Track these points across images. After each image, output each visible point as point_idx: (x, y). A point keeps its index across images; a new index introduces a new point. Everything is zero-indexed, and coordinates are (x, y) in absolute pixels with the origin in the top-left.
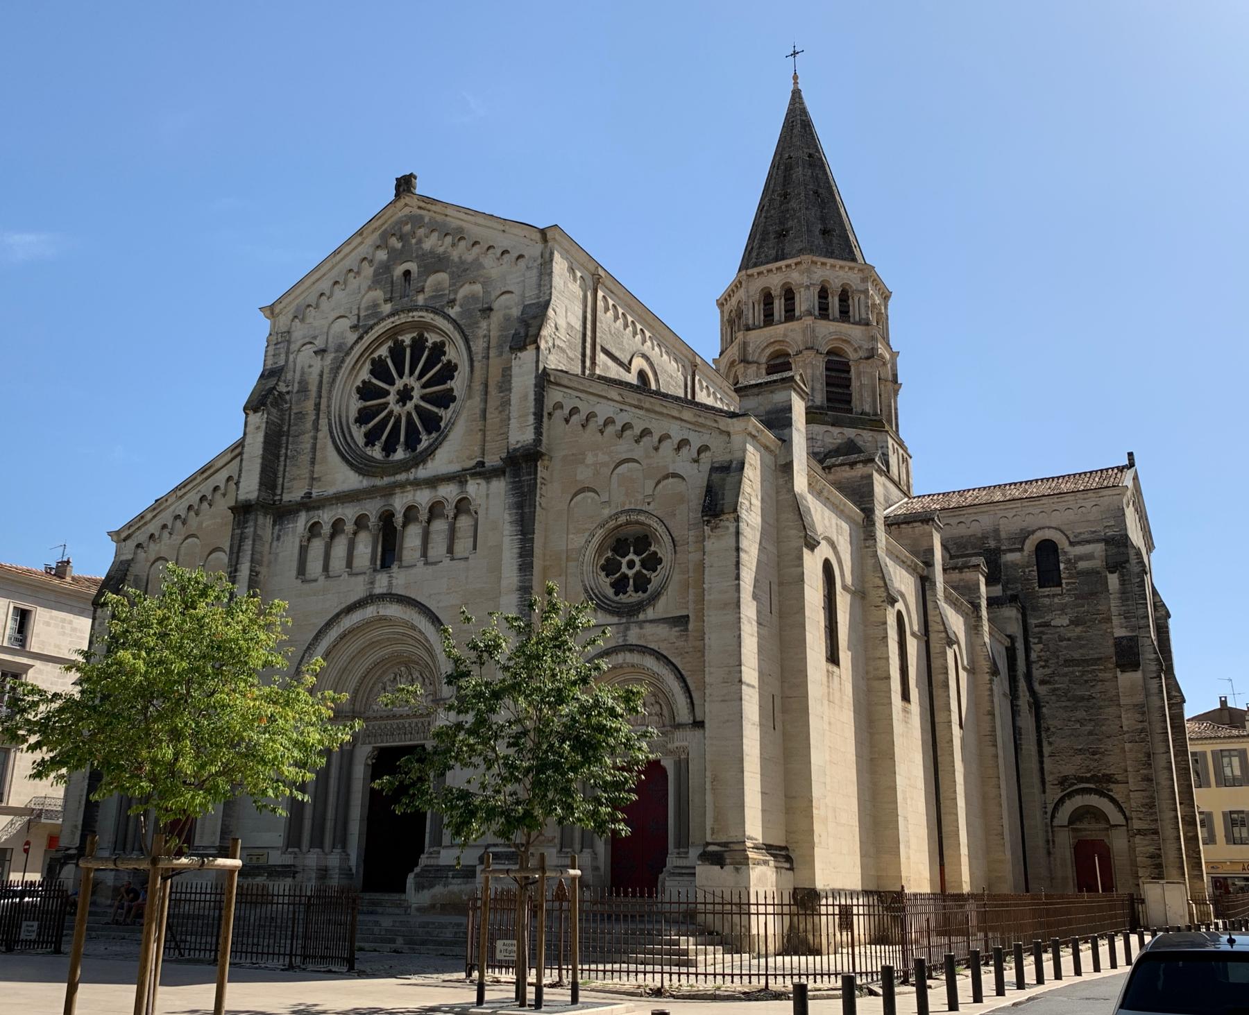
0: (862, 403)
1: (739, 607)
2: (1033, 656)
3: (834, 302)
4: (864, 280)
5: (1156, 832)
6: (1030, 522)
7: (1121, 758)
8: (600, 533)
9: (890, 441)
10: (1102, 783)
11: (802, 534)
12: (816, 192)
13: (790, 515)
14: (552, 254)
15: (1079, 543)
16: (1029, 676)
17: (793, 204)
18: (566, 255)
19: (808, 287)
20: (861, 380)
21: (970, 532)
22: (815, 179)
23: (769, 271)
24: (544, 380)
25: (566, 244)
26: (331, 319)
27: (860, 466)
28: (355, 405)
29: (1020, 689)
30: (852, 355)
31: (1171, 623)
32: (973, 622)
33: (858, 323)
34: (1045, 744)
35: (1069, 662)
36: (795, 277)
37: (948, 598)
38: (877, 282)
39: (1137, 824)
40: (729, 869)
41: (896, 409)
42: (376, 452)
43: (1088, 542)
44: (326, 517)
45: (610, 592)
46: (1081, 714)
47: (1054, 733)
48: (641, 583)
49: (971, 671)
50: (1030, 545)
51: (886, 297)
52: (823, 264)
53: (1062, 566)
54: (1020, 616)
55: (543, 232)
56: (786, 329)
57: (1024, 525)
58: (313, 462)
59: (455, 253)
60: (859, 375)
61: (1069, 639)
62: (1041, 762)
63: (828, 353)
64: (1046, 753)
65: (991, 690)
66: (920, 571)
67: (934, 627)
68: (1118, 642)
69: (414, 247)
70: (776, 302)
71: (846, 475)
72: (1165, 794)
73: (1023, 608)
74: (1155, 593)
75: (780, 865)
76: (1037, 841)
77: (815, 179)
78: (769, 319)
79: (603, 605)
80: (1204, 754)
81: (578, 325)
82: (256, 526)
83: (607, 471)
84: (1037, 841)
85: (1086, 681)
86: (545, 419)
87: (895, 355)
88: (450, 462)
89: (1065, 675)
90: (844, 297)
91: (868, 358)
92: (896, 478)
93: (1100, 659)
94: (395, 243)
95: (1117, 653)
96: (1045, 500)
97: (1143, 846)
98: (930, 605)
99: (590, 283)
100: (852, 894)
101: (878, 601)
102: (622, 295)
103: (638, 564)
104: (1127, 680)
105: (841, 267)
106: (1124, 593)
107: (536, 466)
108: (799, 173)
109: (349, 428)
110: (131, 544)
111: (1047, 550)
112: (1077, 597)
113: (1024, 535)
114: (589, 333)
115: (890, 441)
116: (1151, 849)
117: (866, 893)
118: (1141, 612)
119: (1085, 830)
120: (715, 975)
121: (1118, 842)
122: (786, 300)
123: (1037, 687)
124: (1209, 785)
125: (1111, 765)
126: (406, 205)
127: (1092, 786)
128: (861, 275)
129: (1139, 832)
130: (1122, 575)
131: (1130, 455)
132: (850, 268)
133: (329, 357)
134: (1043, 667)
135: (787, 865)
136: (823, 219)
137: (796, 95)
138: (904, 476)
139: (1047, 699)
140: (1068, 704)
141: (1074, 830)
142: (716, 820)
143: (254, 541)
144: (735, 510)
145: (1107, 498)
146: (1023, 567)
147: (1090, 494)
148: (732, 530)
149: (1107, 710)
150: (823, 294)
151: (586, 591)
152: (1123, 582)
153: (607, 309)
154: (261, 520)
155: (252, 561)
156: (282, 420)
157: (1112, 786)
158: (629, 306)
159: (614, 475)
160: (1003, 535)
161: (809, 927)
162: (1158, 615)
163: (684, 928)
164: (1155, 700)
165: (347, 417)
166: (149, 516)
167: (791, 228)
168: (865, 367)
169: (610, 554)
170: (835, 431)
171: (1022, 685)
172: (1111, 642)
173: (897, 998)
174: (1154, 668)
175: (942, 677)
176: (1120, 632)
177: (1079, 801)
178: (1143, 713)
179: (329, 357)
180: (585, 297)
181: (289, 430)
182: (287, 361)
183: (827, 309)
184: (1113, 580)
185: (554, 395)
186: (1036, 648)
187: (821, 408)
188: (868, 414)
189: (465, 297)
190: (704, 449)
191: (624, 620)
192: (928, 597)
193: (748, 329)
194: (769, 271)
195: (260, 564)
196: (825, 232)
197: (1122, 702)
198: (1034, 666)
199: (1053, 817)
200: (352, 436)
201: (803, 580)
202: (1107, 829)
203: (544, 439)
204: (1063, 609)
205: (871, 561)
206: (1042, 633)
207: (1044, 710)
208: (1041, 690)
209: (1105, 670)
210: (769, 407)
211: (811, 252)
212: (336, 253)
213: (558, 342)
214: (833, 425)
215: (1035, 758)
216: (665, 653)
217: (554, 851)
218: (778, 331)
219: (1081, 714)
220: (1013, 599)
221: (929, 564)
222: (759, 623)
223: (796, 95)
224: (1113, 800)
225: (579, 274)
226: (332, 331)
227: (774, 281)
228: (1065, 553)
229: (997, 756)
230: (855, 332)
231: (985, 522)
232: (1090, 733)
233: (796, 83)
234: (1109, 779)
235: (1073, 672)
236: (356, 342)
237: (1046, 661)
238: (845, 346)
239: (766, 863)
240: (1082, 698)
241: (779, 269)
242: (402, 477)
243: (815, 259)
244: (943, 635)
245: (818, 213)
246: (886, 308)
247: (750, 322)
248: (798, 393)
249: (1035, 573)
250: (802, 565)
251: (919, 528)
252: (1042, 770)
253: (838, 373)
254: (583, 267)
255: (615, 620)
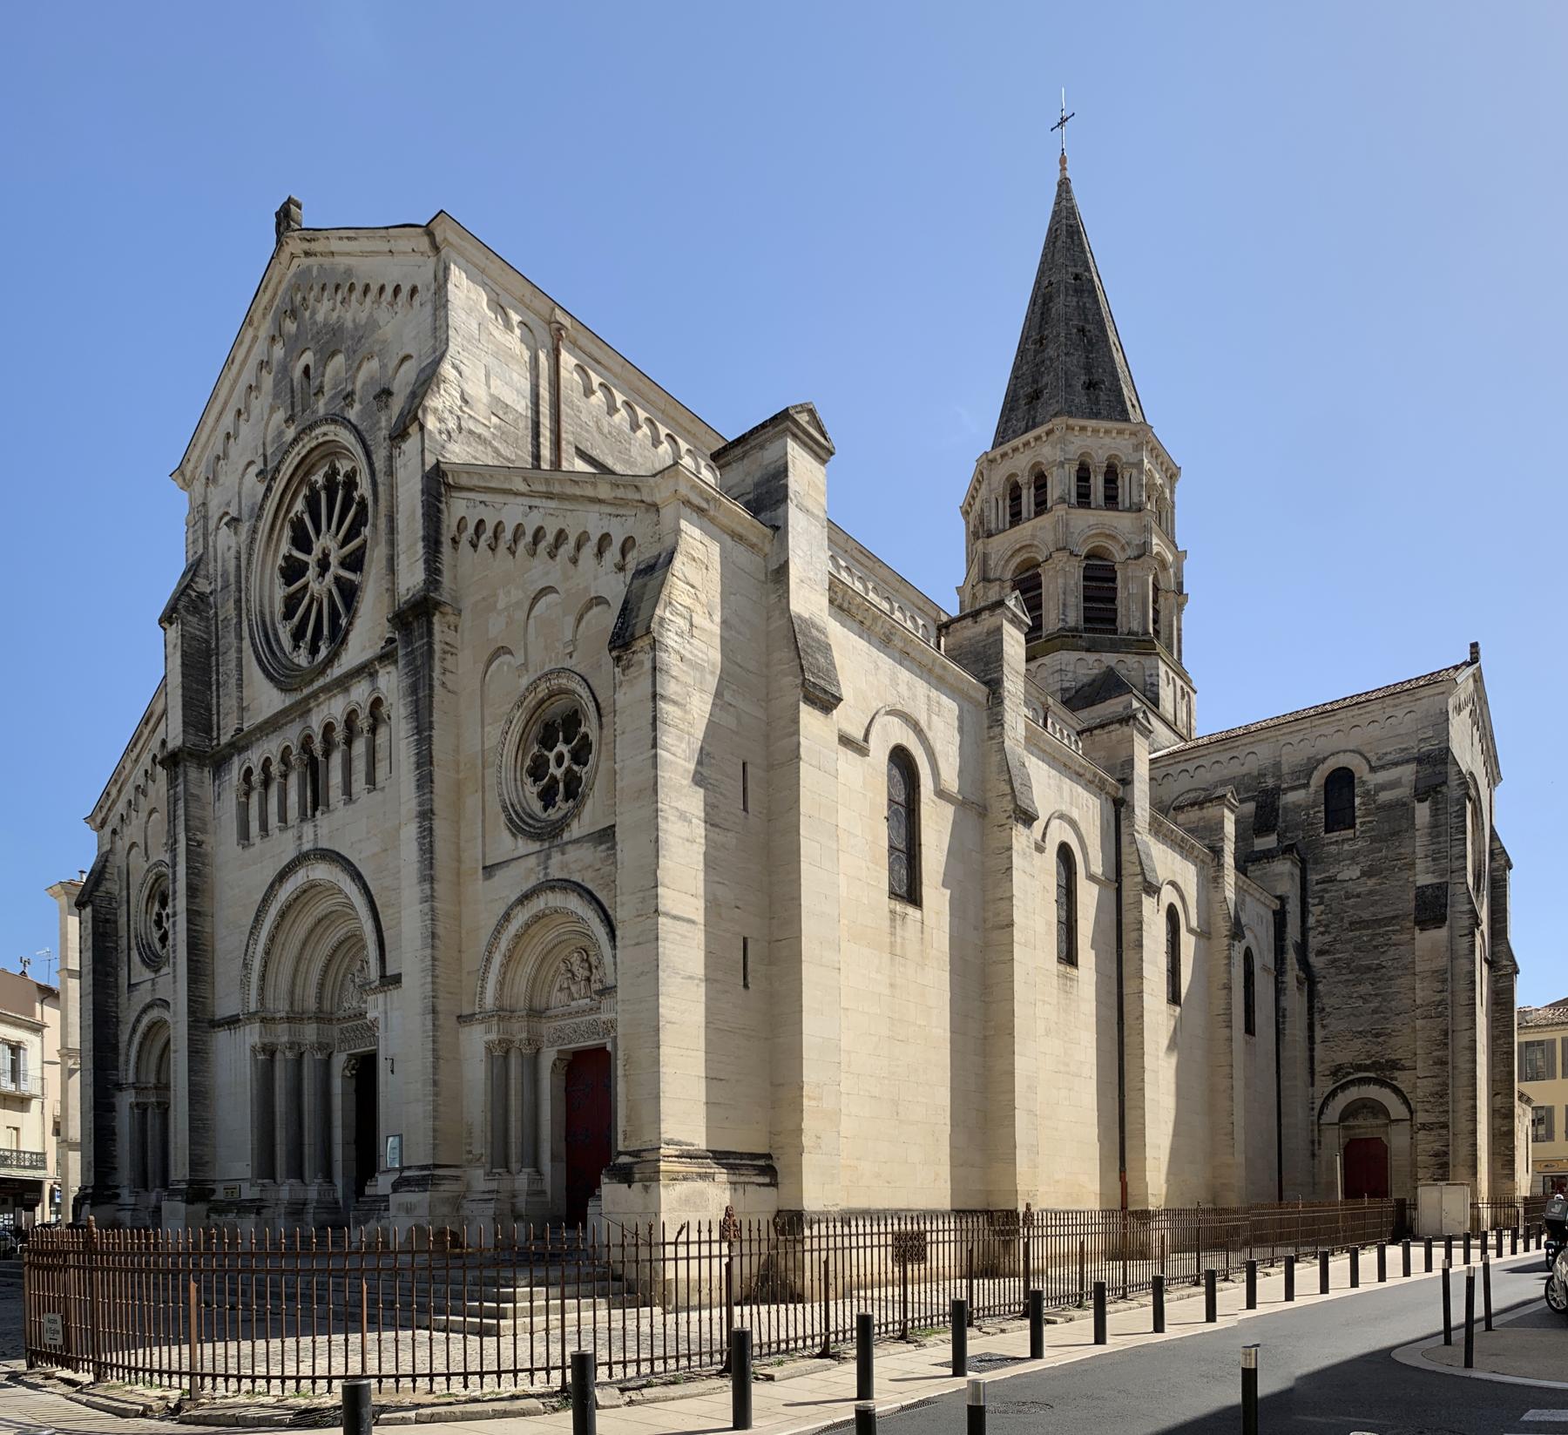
0: (1130, 616)
1: (656, 792)
2: (1311, 921)
3: (1097, 484)
4: (1138, 448)
5: (1445, 1126)
6: (1323, 746)
7: (1412, 1041)
8: (519, 717)
9: (1162, 668)
10: (1384, 1071)
11: (799, 681)
12: (1082, 330)
13: (786, 654)
14: (446, 269)
15: (1382, 767)
16: (1302, 948)
17: (1051, 352)
18: (479, 275)
19: (1062, 464)
20: (1132, 592)
21: (1245, 770)
22: (1082, 310)
23: (1015, 450)
24: (438, 483)
25: (479, 256)
26: (241, 468)
27: (985, 615)
28: (280, 592)
29: (1288, 961)
30: (1119, 556)
31: (1513, 877)
32: (1212, 872)
33: (1129, 510)
34: (1318, 1028)
35: (1356, 925)
36: (1048, 453)
37: (1156, 829)
38: (1157, 452)
39: (1421, 1117)
40: (637, 1186)
41: (1179, 630)
42: (302, 658)
43: (1396, 764)
44: (254, 757)
45: (537, 806)
46: (1365, 989)
47: (1329, 1014)
48: (573, 787)
49: (1204, 934)
50: (1318, 778)
51: (1173, 475)
52: (1083, 429)
53: (1357, 801)
54: (1297, 872)
55: (428, 230)
56: (1034, 528)
57: (1311, 752)
58: (240, 686)
59: (349, 316)
60: (1126, 581)
61: (1358, 896)
62: (1312, 1050)
63: (1087, 557)
64: (1318, 1039)
65: (1229, 957)
66: (1109, 789)
67: (1129, 868)
68: (1421, 890)
69: (308, 322)
70: (1024, 492)
71: (968, 633)
72: (1464, 1080)
73: (1303, 861)
74: (1494, 836)
75: (734, 1179)
76: (1297, 1141)
77: (1082, 310)
78: (1016, 517)
79: (520, 825)
80: (1553, 1042)
81: (522, 406)
82: (186, 782)
83: (520, 615)
84: (1297, 1141)
85: (1376, 947)
86: (446, 548)
87: (1180, 556)
88: (363, 650)
89: (1351, 941)
90: (1111, 477)
91: (1138, 557)
92: (1170, 717)
93: (1394, 918)
94: (290, 326)
95: (1417, 906)
96: (1341, 715)
97: (1427, 1143)
98: (1125, 839)
99: (544, 336)
100: (933, 1215)
101: (1002, 818)
102: (618, 370)
103: (567, 757)
104: (1429, 941)
105: (1107, 432)
106: (1435, 827)
107: (430, 623)
108: (1059, 306)
109: (273, 624)
110: (108, 829)
111: (1341, 781)
112: (1373, 840)
113: (1313, 764)
114: (545, 422)
115: (1162, 668)
116: (1437, 1146)
117: (959, 1213)
118: (1456, 850)
119: (1359, 1127)
120: (283, 1379)
121: (1398, 1140)
122: (1037, 489)
123: (1313, 959)
124: (1553, 1077)
125: (1398, 1048)
126: (293, 256)
127: (1372, 1075)
128: (1134, 440)
129: (1424, 1126)
130: (1435, 802)
131: (1474, 646)
132: (1120, 432)
133: (245, 528)
134: (1322, 934)
135: (767, 1180)
136: (1088, 369)
137: (1064, 184)
138: (1182, 715)
139: (1324, 973)
140: (1351, 977)
141: (1347, 1128)
142: (629, 1119)
143: (186, 802)
144: (648, 631)
145: (1427, 702)
146: (1308, 808)
147: (1404, 697)
148: (648, 665)
149: (1399, 981)
150: (1083, 474)
151: (505, 809)
152: (1435, 812)
153: (588, 392)
154: (193, 774)
155: (187, 829)
156: (209, 633)
157: (1397, 1074)
158: (638, 392)
159: (531, 621)
160: (1285, 769)
161: (791, 1264)
162: (1495, 865)
163: (539, 1273)
164: (1463, 963)
165: (272, 613)
166: (114, 792)
167: (1046, 386)
168: (1134, 570)
169: (535, 749)
170: (1091, 657)
171: (1291, 957)
172: (1412, 895)
173: (1166, 1305)
174: (1467, 923)
175: (1134, 935)
176: (1424, 880)
177: (1354, 1093)
178: (1445, 981)
179: (245, 528)
180: (535, 360)
181: (217, 647)
182: (206, 548)
183: (1087, 496)
184: (1423, 811)
185: (458, 508)
186: (1315, 911)
187: (1076, 629)
188: (1136, 634)
189: (365, 384)
190: (628, 545)
191: (546, 845)
192: (1123, 829)
193: (990, 535)
194: (1015, 450)
195: (204, 831)
196: (1091, 386)
197: (1418, 969)
198: (1311, 934)
199: (1321, 1112)
200: (278, 640)
201: (798, 757)
202: (1386, 1125)
203: (446, 579)
204: (1353, 858)
205: (995, 758)
206: (1325, 890)
207: (1320, 987)
208: (1317, 962)
209: (1400, 932)
210: (758, 476)
211: (1070, 414)
212: (230, 361)
213: (468, 424)
214: (1088, 650)
215: (1304, 1044)
216: (590, 886)
217: (481, 1172)
218: (1025, 530)
219: (1365, 989)
220: (1289, 849)
221: (1126, 782)
222: (710, 822)
223: (1064, 184)
224: (1396, 1090)
225: (515, 318)
226: (244, 489)
227: (1021, 465)
228: (1364, 783)
229: (1230, 1040)
230: (1121, 522)
231: (1263, 754)
232: (1375, 1011)
233: (1063, 169)
234: (1394, 1065)
235: (1359, 937)
236: (265, 497)
237: (1327, 926)
238: (1109, 544)
239: (711, 1177)
240: (1369, 969)
241: (1027, 444)
242: (321, 682)
243: (1071, 421)
244: (1139, 878)
245: (1083, 360)
246: (1172, 492)
247: (993, 526)
248: (804, 445)
249: (1322, 815)
250: (797, 732)
251: (1118, 731)
252: (1312, 1059)
253: (1100, 580)
254: (523, 305)
255: (536, 846)
